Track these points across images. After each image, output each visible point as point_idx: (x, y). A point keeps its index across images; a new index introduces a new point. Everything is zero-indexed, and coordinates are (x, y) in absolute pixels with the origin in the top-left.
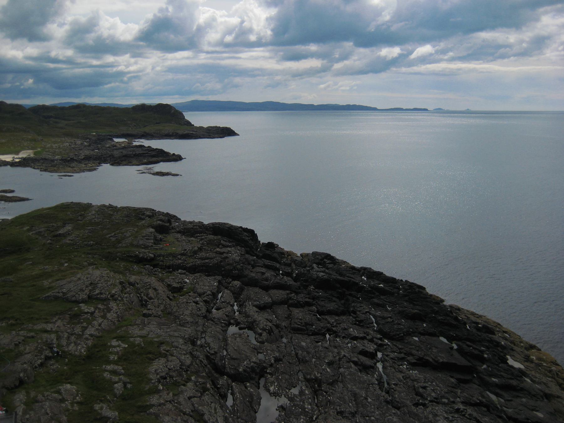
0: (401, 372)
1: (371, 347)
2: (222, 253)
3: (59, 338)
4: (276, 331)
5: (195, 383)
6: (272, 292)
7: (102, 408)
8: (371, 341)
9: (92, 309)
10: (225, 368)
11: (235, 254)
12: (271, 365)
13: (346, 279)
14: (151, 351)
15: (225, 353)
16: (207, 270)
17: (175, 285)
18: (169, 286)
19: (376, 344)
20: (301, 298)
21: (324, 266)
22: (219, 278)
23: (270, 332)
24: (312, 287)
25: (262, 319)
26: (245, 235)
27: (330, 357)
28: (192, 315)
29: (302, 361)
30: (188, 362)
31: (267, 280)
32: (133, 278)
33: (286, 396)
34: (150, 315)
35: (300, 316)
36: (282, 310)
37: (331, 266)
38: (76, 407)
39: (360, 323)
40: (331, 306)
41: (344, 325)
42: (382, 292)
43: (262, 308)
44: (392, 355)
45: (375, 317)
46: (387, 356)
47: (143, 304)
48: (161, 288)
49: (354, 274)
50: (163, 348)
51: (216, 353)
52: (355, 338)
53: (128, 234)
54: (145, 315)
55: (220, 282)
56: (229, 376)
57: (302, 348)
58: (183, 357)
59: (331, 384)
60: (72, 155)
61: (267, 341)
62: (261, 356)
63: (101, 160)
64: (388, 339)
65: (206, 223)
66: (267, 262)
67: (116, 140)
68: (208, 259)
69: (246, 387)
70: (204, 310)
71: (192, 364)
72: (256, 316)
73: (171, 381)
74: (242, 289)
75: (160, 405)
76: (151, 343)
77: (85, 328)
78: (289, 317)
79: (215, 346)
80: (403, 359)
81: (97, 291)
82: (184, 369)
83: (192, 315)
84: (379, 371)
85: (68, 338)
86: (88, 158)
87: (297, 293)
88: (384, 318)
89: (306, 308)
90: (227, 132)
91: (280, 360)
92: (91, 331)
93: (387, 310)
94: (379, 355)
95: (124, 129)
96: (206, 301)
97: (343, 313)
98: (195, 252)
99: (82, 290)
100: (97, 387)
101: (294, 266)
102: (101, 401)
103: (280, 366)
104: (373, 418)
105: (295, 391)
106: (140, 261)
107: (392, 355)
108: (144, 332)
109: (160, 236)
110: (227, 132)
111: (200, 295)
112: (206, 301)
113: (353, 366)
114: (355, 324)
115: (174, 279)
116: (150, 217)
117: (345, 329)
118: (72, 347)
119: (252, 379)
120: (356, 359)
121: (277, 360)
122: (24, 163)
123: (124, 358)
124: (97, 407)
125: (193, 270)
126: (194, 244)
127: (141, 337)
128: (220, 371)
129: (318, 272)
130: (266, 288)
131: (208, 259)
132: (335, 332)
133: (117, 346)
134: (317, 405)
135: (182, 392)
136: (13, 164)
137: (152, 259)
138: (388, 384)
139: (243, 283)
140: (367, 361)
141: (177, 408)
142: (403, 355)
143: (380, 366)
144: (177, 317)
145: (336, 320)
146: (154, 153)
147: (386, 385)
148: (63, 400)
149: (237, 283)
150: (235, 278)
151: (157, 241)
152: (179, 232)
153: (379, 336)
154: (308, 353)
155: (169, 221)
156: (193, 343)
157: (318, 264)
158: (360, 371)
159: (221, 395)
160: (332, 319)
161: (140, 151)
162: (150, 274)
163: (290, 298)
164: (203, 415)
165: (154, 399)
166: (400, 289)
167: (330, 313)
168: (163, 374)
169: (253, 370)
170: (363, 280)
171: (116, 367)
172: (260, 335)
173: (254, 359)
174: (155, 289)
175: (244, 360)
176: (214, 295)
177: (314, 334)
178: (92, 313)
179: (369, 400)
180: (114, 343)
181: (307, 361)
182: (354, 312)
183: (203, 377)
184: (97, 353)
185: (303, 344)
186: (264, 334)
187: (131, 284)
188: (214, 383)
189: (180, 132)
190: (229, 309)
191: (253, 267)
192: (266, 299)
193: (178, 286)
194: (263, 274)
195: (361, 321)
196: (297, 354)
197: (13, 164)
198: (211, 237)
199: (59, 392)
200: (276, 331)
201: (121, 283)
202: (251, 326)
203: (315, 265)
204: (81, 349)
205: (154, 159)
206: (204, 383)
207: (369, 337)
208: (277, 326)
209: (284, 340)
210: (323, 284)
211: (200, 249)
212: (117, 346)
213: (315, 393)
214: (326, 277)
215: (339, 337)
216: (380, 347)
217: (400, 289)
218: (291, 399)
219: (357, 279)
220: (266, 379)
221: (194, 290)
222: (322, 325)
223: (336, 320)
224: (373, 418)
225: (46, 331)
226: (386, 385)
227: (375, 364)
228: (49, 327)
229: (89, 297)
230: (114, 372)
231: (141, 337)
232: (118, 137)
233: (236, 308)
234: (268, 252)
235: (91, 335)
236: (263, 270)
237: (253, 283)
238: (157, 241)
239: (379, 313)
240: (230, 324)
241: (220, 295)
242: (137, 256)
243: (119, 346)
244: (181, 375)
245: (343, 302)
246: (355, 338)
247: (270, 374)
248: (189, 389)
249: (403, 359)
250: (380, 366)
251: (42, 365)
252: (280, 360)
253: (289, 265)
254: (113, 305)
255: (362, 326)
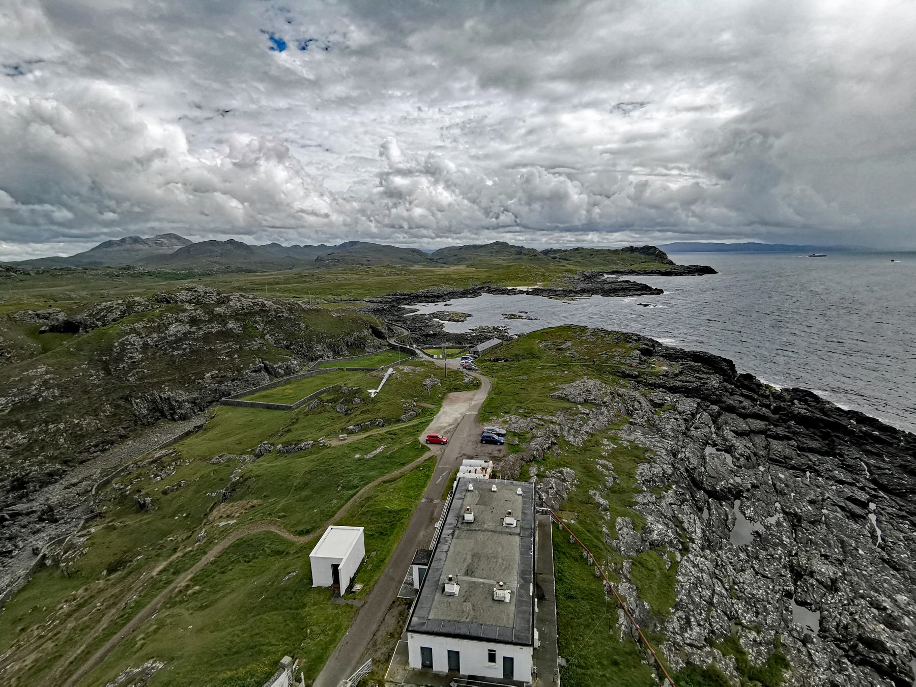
0: (901, 531)
1: (863, 497)
2: (702, 379)
3: (562, 429)
4: (754, 459)
5: (676, 492)
6: (750, 420)
7: (595, 494)
8: (862, 489)
9: (587, 411)
10: (702, 483)
11: (714, 381)
12: (748, 490)
13: (831, 420)
14: (639, 455)
15: (703, 470)
16: (688, 392)
17: (657, 401)
18: (651, 401)
19: (869, 493)
20: (780, 431)
21: (806, 404)
22: (699, 400)
23: (748, 458)
24: (793, 422)
25: (740, 445)
26: (724, 366)
27: (812, 496)
28: (673, 430)
29: (780, 493)
30: (670, 472)
31: (744, 408)
32: (622, 391)
33: (762, 522)
34: (635, 424)
35: (780, 448)
36: (760, 440)
37: (813, 404)
38: (574, 489)
39: (849, 468)
40: (814, 444)
41: (826, 466)
42: (877, 440)
43: (740, 434)
44: (889, 510)
45: (867, 464)
46: (883, 509)
47: (630, 413)
48: (645, 404)
49: (840, 415)
50: (648, 455)
51: (695, 468)
52: (841, 482)
53: (617, 354)
54: (631, 423)
55: (698, 404)
56: (706, 491)
57: (780, 480)
58: (665, 466)
59: (813, 523)
60: (571, 288)
61: (744, 466)
62: (738, 480)
63: (593, 292)
64: (883, 491)
65: (687, 350)
66: (745, 392)
67: (606, 276)
68: (687, 382)
69: (722, 505)
70: (683, 428)
71: (673, 474)
72: (734, 441)
73: (657, 485)
74: (719, 414)
75: (644, 504)
76: (637, 448)
77: (581, 426)
78: (767, 447)
79: (694, 462)
80: (903, 517)
81: (592, 397)
82: (665, 477)
83: (673, 430)
84: (871, 524)
85: (569, 431)
86: (583, 291)
87: (776, 426)
88: (879, 468)
89: (785, 442)
90: (708, 270)
91: (758, 487)
92: (586, 428)
93: (884, 461)
94: (872, 506)
95: (614, 267)
96: (685, 420)
97: (827, 454)
98: (676, 375)
99: (579, 394)
100: (590, 475)
101: (772, 399)
102: (595, 489)
103: (758, 493)
104: (864, 572)
105: (772, 520)
106: (625, 376)
107: (889, 510)
108: (632, 438)
109: (644, 358)
110: (708, 270)
111: (680, 413)
112: (685, 420)
113: (839, 510)
114: (842, 468)
115: (657, 395)
116: (636, 341)
117: (829, 470)
118: (571, 439)
119: (729, 499)
120: (843, 504)
121: (754, 486)
122: (536, 292)
123: (613, 455)
124: (591, 492)
125: (673, 390)
126: (676, 368)
127: (628, 441)
128: (698, 485)
129: (799, 408)
130: (744, 416)
131: (687, 382)
132: (816, 471)
133: (608, 446)
134: (795, 540)
135: (663, 497)
136: (528, 293)
137: (636, 377)
138: (883, 539)
139: (721, 408)
140: (858, 510)
141: (659, 510)
142: (904, 513)
143: (873, 517)
144: (659, 430)
145: (819, 459)
146: (638, 287)
147: (880, 540)
148: (564, 480)
149: (715, 408)
150: (714, 402)
151: (642, 362)
152: (662, 356)
153: (872, 486)
154: (787, 486)
155: (653, 346)
156: (675, 455)
157: (800, 400)
158: (848, 518)
159: (698, 508)
160: (814, 458)
161: (626, 285)
162: (635, 389)
163: (769, 429)
164: (682, 522)
165: (639, 498)
166: (900, 441)
167: (811, 450)
168: (648, 478)
169: (730, 490)
170: (851, 424)
171: (606, 462)
172: (738, 459)
173: (731, 481)
174: (639, 402)
175: (722, 480)
176: (693, 415)
177: (793, 468)
178: (587, 414)
179: (861, 552)
180: (605, 442)
181: (785, 494)
182: (841, 456)
183: (683, 488)
184: (591, 445)
185: (782, 476)
186: (742, 459)
187: (619, 395)
188: (692, 496)
189: (663, 270)
190: (707, 430)
191: (732, 394)
192: (743, 426)
193: (660, 402)
194: (741, 402)
195: (849, 466)
196: (774, 485)
197: (528, 293)
198: (692, 363)
199: (561, 472)
200: (754, 459)
201: (611, 393)
202: (729, 450)
203: (796, 401)
204: (578, 441)
205: (639, 292)
206: (683, 494)
207: (860, 485)
208: (755, 454)
209: (761, 468)
210: (801, 420)
211: (681, 373)
212: (608, 446)
213: (794, 527)
214: (809, 414)
215: (822, 477)
216: (874, 498)
217: (900, 441)
218: (767, 528)
219: (844, 422)
220: (742, 502)
221: (674, 408)
222: (803, 461)
223: (819, 459)
224: (864, 572)
225: (552, 423)
226: (880, 540)
227: (867, 514)
228: (554, 419)
229: (586, 401)
230: (603, 466)
231: (628, 441)
232: (607, 273)
233: (713, 430)
234: (746, 382)
235: (586, 432)
236: (742, 399)
237: (731, 409)
238: (642, 362)
239: (872, 461)
240: (707, 444)
241: (698, 416)
242: (623, 372)
243: (609, 445)
244: (663, 482)
245: (827, 442)
246: (841, 482)
247: (746, 498)
248: (670, 496)
249: (903, 517)
250: (873, 517)
251: (549, 448)
252: (758, 487)
253: (767, 397)
254: (604, 409)
255: (851, 472)
